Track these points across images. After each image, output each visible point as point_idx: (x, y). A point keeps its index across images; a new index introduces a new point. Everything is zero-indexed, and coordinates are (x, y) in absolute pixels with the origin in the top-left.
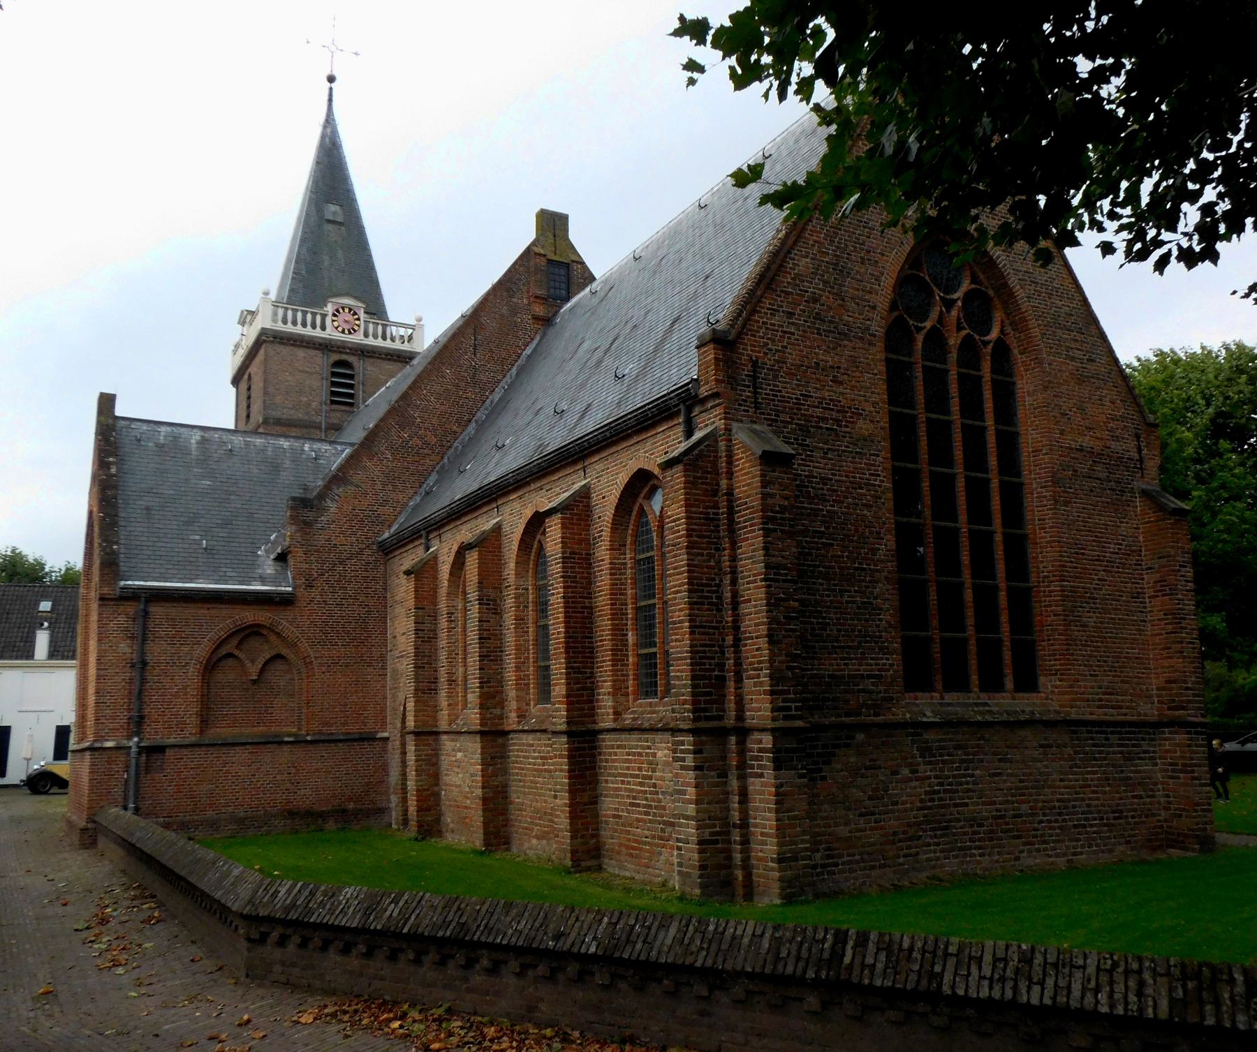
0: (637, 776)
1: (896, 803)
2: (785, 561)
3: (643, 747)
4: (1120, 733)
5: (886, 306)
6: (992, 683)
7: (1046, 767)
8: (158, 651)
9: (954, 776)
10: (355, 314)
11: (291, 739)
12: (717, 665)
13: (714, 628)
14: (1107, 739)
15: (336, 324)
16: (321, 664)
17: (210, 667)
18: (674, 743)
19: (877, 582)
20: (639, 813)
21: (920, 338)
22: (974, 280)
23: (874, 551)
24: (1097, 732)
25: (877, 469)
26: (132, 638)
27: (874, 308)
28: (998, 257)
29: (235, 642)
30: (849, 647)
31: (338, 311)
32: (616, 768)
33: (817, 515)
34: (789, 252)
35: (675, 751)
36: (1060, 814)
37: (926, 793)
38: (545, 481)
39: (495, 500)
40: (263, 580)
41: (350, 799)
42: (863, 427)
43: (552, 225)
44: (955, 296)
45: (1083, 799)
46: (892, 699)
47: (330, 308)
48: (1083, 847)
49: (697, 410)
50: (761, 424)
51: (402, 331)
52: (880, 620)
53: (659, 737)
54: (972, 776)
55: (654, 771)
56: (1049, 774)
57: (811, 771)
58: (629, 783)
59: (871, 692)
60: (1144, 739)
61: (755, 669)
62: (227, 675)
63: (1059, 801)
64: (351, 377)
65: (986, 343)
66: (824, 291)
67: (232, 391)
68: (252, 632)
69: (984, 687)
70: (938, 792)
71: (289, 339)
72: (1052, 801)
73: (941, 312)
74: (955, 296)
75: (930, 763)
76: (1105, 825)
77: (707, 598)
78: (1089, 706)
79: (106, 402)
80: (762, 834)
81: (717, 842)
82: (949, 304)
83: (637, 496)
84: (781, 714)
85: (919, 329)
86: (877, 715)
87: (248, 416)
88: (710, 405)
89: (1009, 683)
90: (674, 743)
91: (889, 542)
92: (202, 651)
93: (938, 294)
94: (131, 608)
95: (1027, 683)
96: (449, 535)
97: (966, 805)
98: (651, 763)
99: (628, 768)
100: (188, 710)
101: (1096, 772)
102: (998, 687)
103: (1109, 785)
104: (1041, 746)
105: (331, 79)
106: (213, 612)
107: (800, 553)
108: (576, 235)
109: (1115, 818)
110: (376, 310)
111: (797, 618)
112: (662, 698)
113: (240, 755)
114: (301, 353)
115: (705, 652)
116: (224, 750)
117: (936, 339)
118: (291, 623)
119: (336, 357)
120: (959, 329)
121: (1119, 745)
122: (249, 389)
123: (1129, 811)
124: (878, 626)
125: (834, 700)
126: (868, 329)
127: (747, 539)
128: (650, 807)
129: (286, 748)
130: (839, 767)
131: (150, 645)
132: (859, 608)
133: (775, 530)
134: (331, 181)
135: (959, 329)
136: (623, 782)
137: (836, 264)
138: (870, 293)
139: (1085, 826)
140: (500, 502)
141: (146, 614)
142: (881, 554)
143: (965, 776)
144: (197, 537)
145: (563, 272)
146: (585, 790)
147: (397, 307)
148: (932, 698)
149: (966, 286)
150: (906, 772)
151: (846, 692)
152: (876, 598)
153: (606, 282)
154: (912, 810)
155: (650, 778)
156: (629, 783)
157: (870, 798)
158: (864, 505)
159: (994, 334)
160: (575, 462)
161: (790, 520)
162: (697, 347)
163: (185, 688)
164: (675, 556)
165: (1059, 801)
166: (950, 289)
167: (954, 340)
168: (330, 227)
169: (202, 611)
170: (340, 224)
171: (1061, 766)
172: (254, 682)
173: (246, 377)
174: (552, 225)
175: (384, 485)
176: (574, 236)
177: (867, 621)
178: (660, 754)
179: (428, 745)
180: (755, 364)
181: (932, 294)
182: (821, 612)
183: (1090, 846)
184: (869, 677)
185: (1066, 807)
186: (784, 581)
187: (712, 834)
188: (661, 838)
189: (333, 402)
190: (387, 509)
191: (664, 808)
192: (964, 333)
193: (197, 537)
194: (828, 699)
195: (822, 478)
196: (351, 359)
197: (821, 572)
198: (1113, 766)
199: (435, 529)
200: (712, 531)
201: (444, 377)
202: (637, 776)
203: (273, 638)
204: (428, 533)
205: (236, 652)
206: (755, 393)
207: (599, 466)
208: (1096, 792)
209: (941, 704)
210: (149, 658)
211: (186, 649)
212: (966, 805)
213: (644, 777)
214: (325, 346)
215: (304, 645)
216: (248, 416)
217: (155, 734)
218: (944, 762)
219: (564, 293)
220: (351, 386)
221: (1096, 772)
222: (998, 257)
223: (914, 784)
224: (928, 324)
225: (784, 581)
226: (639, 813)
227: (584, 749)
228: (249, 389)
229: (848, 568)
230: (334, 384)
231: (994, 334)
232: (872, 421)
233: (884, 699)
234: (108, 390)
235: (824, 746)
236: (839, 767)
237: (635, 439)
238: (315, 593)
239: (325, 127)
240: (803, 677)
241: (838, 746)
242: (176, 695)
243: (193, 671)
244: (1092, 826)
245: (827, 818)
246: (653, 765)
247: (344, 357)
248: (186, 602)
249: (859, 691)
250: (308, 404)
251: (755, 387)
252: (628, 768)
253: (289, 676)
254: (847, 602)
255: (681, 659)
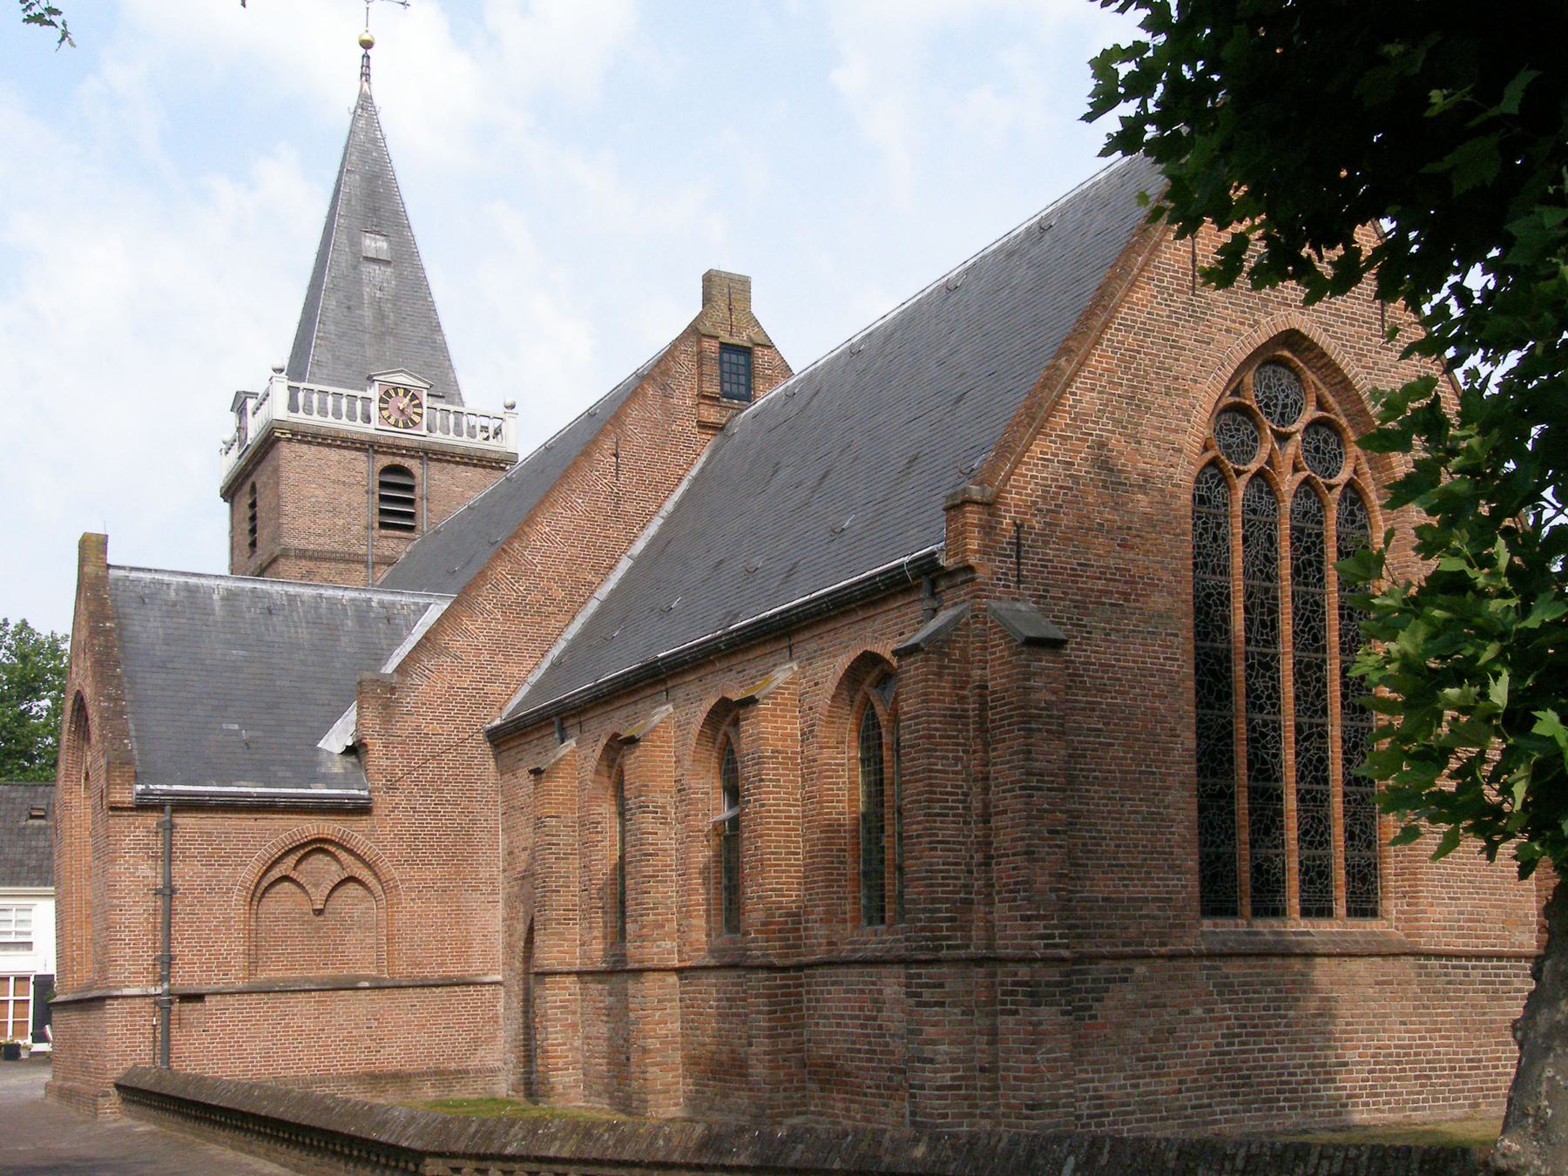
0: (857, 1017)
1: (1185, 1047)
2: (1050, 766)
3: (865, 983)
4: (1484, 968)
5: (1198, 448)
6: (1317, 908)
7: (1384, 1007)
8: (186, 873)
9: (1260, 1017)
10: (414, 397)
11: (367, 984)
12: (964, 886)
13: (960, 843)
14: (1467, 975)
15: (386, 413)
16: (411, 889)
17: (260, 892)
18: (909, 976)
19: (1168, 788)
20: (860, 1060)
21: (1241, 483)
22: (1321, 405)
23: (1167, 751)
24: (1454, 967)
25: (1177, 659)
26: (155, 858)
27: (1180, 451)
28: (1356, 375)
29: (292, 860)
30: (1130, 865)
31: (387, 392)
32: (830, 1008)
33: (1093, 710)
34: (1068, 385)
35: (908, 986)
36: (1398, 1063)
37: (1223, 1036)
38: (734, 661)
39: (664, 681)
40: (328, 780)
41: (450, 1059)
42: (1159, 601)
43: (724, 292)
44: (1292, 428)
45: (1430, 1046)
46: (1183, 926)
47: (374, 392)
48: (1424, 1100)
49: (943, 584)
50: (1025, 601)
51: (479, 422)
52: (1172, 833)
53: (884, 971)
54: (1285, 1017)
55: (880, 1010)
56: (1385, 1015)
57: (1076, 1009)
58: (846, 1026)
59: (1154, 918)
60: (1516, 976)
61: (1012, 891)
62: (283, 900)
63: (1396, 1047)
64: (410, 488)
65: (1330, 488)
66: (1113, 432)
67: (226, 507)
68: (317, 846)
69: (1305, 913)
70: (1239, 1035)
71: (315, 436)
72: (1389, 1047)
73: (1273, 449)
74: (1292, 428)
75: (1230, 1001)
76: (1456, 1076)
77: (952, 808)
78: (1445, 936)
79: (92, 548)
80: (1015, 1078)
81: (959, 1087)
82: (1283, 438)
83: (861, 683)
84: (1042, 942)
85: (1239, 473)
86: (1163, 944)
87: (253, 544)
88: (960, 579)
89: (1340, 907)
90: (909, 976)
91: (1189, 739)
92: (249, 873)
93: (1268, 425)
94: (152, 820)
95: (1364, 905)
96: (594, 724)
97: (1275, 1050)
98: (876, 1001)
99: (846, 1008)
100: (233, 947)
101: (1449, 1014)
102: (1326, 912)
103: (1466, 1030)
104: (1377, 983)
105: (367, 45)
106: (261, 823)
107: (1070, 756)
108: (761, 307)
109: (1470, 1068)
110: (445, 390)
111: (1065, 832)
112: (891, 925)
113: (302, 1005)
114: (334, 455)
115: (948, 871)
116: (283, 997)
117: (1264, 480)
118: (368, 837)
119: (386, 461)
120: (1296, 469)
121: (1482, 983)
122: (253, 505)
123: (1488, 1060)
124: (1168, 840)
125: (1109, 927)
126: (1170, 477)
127: (1004, 740)
128: (874, 1052)
129: (362, 994)
130: (1112, 1003)
131: (177, 867)
132: (1144, 819)
133: (1040, 730)
134: (367, 197)
135: (1296, 469)
136: (838, 1025)
137: (1132, 398)
138: (1176, 431)
139: (1429, 1077)
140: (669, 684)
141: (171, 827)
142: (1177, 755)
143: (1274, 1017)
144: (236, 727)
145: (742, 360)
146: (789, 1035)
147: (481, 387)
148: (1237, 926)
149: (1310, 413)
150: (1198, 1012)
151: (1124, 917)
152: (1167, 807)
153: (810, 378)
154: (1204, 1055)
155: (875, 1018)
156: (846, 1026)
157: (1152, 1041)
158: (1155, 696)
159: (1343, 476)
160: (778, 639)
161: (1059, 717)
162: (947, 509)
163: (227, 920)
164: (913, 759)
165: (1396, 1047)
166: (1284, 419)
167: (1288, 483)
168: (375, 269)
169: (246, 822)
170: (387, 263)
171: (1403, 1007)
172: (319, 912)
173: (247, 488)
174: (724, 292)
175: (493, 653)
176: (757, 309)
177: (1153, 833)
178: (888, 991)
179: (566, 988)
180: (1019, 527)
181: (1258, 427)
182: (1095, 824)
183: (1435, 1100)
184: (1155, 900)
185: (1406, 1055)
186: (1050, 789)
187: (953, 1079)
188: (887, 1088)
189: (383, 525)
190: (496, 687)
191: (892, 1053)
192: (1301, 475)
193: (236, 727)
194: (1102, 926)
195: (1101, 665)
196: (408, 463)
197: (1096, 778)
198: (1473, 1006)
199: (573, 716)
200: (960, 731)
201: (572, 509)
202: (857, 1017)
203: (343, 855)
204: (562, 720)
205: (294, 875)
206: (1019, 564)
207: (812, 646)
208: (1448, 1038)
209: (1248, 933)
210: (177, 882)
211: (227, 871)
212: (1275, 1050)
213: (867, 1018)
214: (368, 447)
215: (385, 866)
216: (253, 544)
217: (183, 979)
218: (1248, 1000)
219: (743, 390)
220: (410, 502)
221: (1449, 1014)
222: (1356, 375)
223: (1207, 1025)
224: (1253, 467)
225: (1050, 789)
226: (860, 1060)
227: (788, 986)
228: (253, 505)
229: (1134, 772)
230: (383, 498)
231: (1343, 476)
232: (1171, 594)
233: (1172, 926)
234: (96, 529)
235: (1094, 981)
236: (1112, 1003)
237: (861, 615)
238: (399, 797)
239: (356, 117)
240: (1070, 900)
241: (1114, 981)
242: (216, 930)
243: (237, 898)
244: (1438, 1077)
245: (1095, 1062)
246: (878, 1003)
247: (398, 461)
248: (226, 811)
249: (1141, 917)
250: (346, 529)
251: (1018, 558)
252: (846, 1008)
253: (366, 905)
254: (1130, 812)
255: (918, 879)
